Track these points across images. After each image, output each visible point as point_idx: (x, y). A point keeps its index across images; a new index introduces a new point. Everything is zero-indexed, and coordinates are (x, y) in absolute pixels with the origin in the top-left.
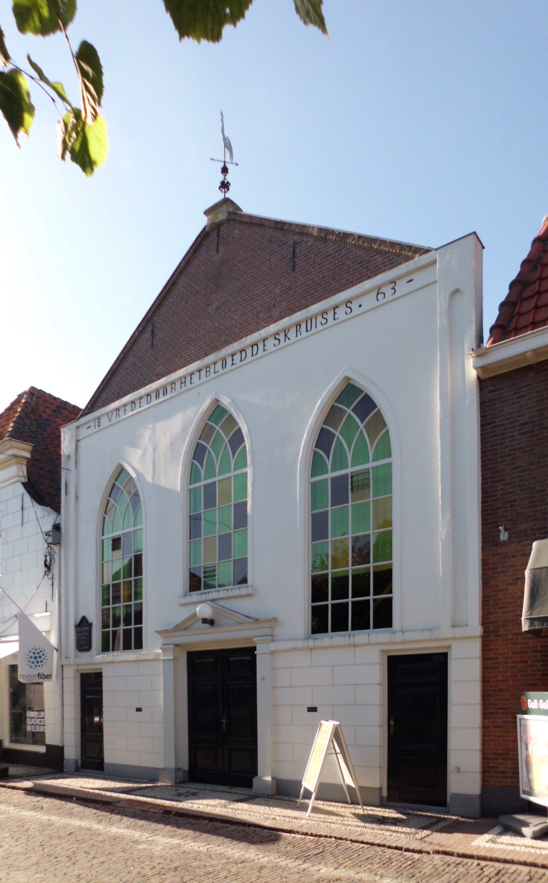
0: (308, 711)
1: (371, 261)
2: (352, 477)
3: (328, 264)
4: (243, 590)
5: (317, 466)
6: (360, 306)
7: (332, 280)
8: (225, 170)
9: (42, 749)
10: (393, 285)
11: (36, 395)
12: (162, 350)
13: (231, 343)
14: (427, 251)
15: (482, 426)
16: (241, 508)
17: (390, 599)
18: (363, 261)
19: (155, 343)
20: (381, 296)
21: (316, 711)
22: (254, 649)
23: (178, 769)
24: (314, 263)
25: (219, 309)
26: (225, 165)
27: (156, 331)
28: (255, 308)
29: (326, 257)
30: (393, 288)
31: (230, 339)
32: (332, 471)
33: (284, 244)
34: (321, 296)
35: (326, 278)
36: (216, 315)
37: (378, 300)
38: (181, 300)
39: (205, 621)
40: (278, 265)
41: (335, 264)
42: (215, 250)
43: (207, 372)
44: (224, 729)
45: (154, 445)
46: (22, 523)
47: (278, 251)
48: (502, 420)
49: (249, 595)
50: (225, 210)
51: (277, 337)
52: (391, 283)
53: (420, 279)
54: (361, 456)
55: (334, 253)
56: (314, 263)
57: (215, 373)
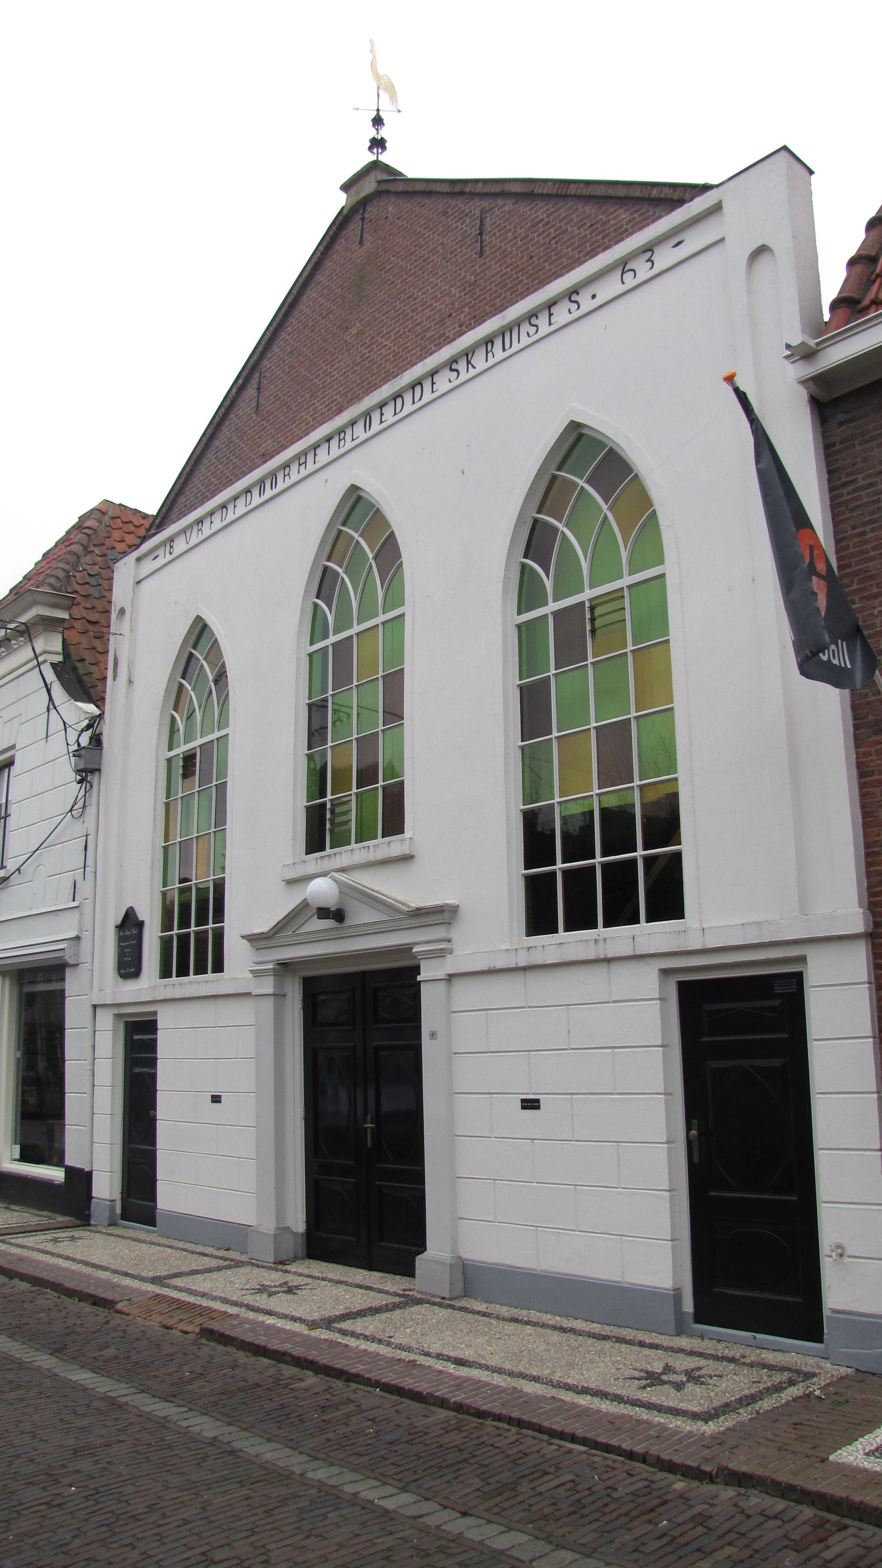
0: (523, 1108)
1: (609, 220)
2: (592, 609)
3: (538, 236)
4: (393, 846)
5: (528, 593)
6: (594, 297)
7: (545, 262)
8: (378, 121)
9: (56, 1174)
10: (649, 254)
11: (109, 514)
12: (289, 421)
13: (380, 386)
14: (706, 188)
15: (831, 489)
16: (394, 683)
17: (678, 856)
18: (596, 223)
19: (262, 401)
20: (628, 276)
21: (538, 1108)
22: (416, 970)
23: (283, 1230)
24: (515, 238)
25: (363, 335)
26: (378, 114)
27: (264, 382)
28: (419, 324)
29: (533, 226)
30: (649, 260)
31: (378, 381)
32: (555, 600)
33: (467, 215)
34: (528, 289)
35: (535, 259)
36: (357, 344)
37: (623, 283)
38: (305, 327)
39: (323, 913)
40: (456, 249)
41: (549, 234)
42: (357, 242)
43: (340, 440)
44: (369, 1144)
45: (248, 577)
46: (47, 737)
47: (457, 227)
48: (870, 476)
49: (407, 858)
50: (373, 180)
51: (454, 366)
52: (645, 252)
53: (694, 241)
54: (606, 566)
55: (548, 217)
56: (515, 238)
57: (353, 440)
